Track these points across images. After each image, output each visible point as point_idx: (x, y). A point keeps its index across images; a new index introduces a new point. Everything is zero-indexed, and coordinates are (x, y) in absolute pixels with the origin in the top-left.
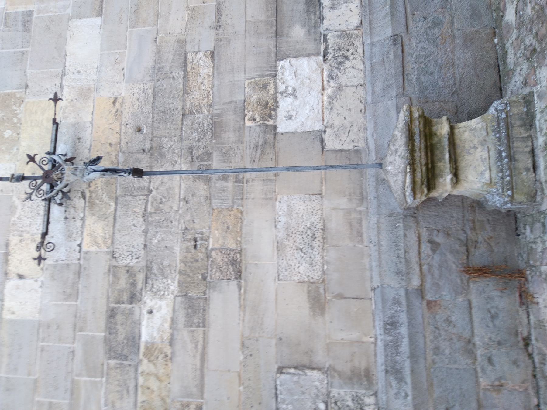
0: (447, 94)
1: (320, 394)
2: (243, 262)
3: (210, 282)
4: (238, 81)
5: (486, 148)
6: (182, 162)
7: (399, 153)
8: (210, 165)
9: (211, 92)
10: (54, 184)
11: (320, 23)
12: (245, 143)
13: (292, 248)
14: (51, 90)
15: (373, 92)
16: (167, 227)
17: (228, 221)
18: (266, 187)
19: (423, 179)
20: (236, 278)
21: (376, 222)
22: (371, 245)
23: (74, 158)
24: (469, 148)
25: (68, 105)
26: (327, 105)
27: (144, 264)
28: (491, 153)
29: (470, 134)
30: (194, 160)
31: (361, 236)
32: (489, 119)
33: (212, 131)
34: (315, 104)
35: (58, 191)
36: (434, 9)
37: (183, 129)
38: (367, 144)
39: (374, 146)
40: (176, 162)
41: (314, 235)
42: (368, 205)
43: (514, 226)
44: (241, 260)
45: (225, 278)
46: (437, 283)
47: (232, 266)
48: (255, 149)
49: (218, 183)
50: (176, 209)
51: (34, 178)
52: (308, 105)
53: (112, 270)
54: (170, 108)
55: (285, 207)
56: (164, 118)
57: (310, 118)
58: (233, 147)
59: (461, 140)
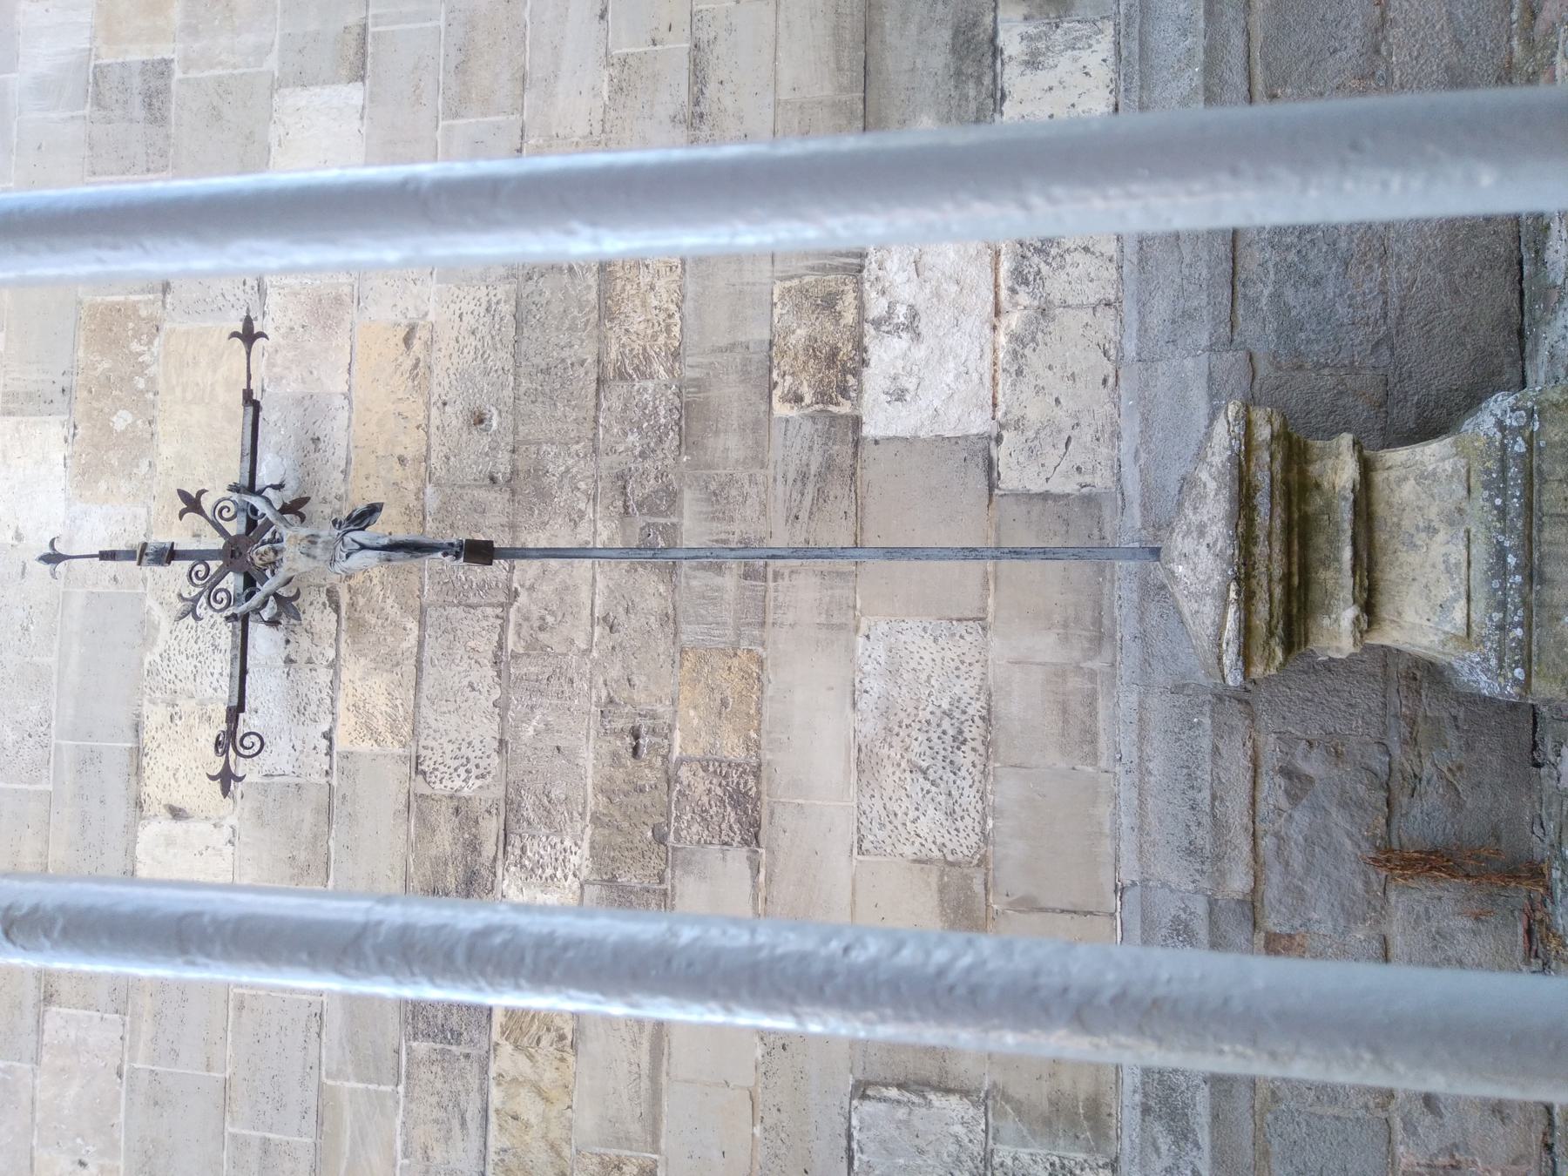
0: (1361, 343)
1: (964, 1157)
2: (765, 798)
3: (674, 849)
4: (754, 284)
5: (1462, 534)
6: (598, 516)
7: (1209, 539)
8: (673, 525)
9: (677, 316)
10: (255, 574)
11: (994, 110)
12: (771, 466)
13: (899, 765)
14: (232, 299)
15: (1143, 330)
16: (560, 694)
17: (725, 685)
18: (829, 592)
19: (1274, 622)
20: (745, 842)
21: (1135, 706)
22: (1118, 769)
23: (304, 501)
24: (1413, 531)
25: (282, 342)
27: (498, 792)
28: (1474, 551)
31: (1093, 742)
32: (1476, 449)
33: (680, 429)
35: (267, 596)
36: (1337, 81)
37: (601, 421)
38: (1119, 480)
39: (1138, 487)
40: (582, 514)
41: (961, 732)
43: (1526, 738)
44: (759, 793)
45: (716, 841)
46: (1297, 887)
47: (734, 807)
48: (799, 483)
49: (695, 577)
50: (584, 647)
51: (201, 556)
52: (951, 358)
53: (414, 805)
54: (563, 360)
55: (880, 652)
56: (547, 389)
57: (956, 397)
58: (737, 476)
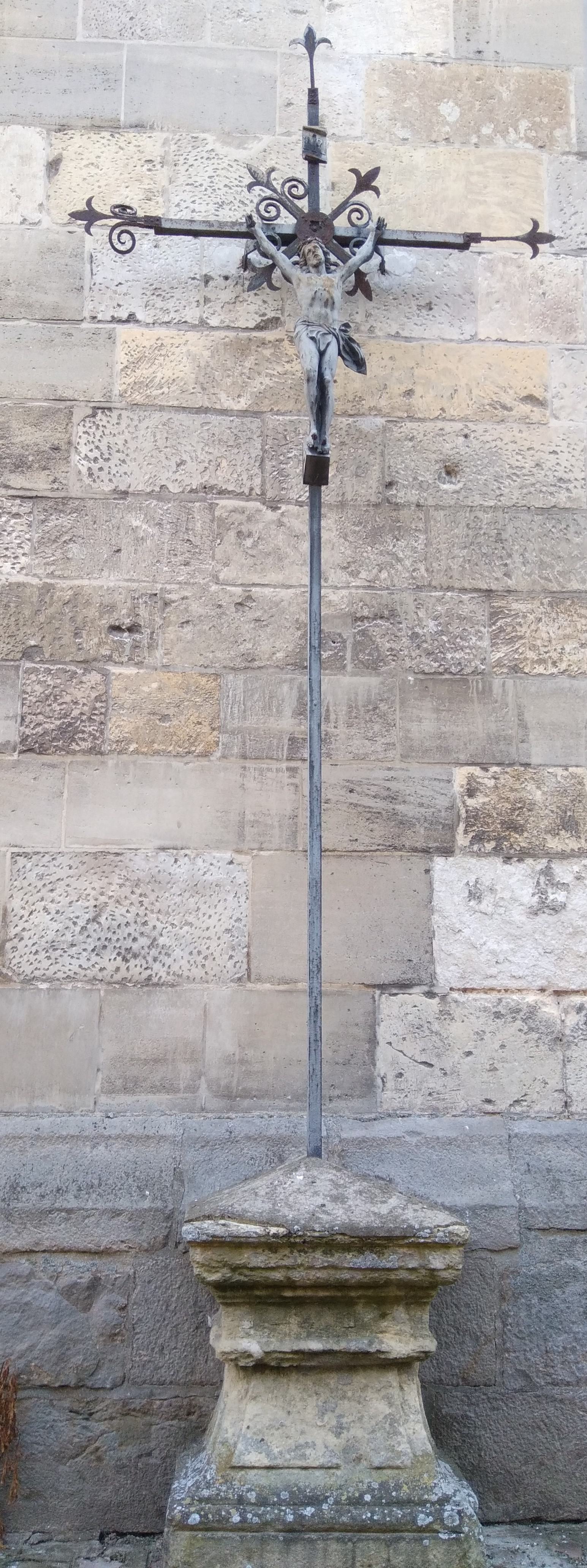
2: (69, 759)
3: (17, 668)
6: (353, 591)
7: (330, 1206)
8: (344, 667)
9: (555, 670)
10: (294, 245)
12: (404, 765)
15: (540, 1140)
16: (173, 552)
17: (182, 718)
20: (24, 739)
22: (98, 1115)
24: (338, 1411)
26: (508, 1003)
27: (75, 490)
28: (318, 1473)
29: (381, 1418)
30: (359, 623)
31: (125, 1090)
32: (421, 1475)
33: (441, 674)
34: (513, 968)
35: (272, 257)
38: (390, 1116)
40: (355, 574)
41: (135, 956)
42: (212, 1111)
43: (129, 1526)
44: (74, 752)
47: (59, 728)
48: (386, 793)
49: (291, 689)
50: (221, 576)
51: (312, 191)
52: (512, 946)
53: (62, 405)
55: (216, 875)
56: (481, 539)
57: (473, 951)
58: (394, 731)
59: (365, 1388)
